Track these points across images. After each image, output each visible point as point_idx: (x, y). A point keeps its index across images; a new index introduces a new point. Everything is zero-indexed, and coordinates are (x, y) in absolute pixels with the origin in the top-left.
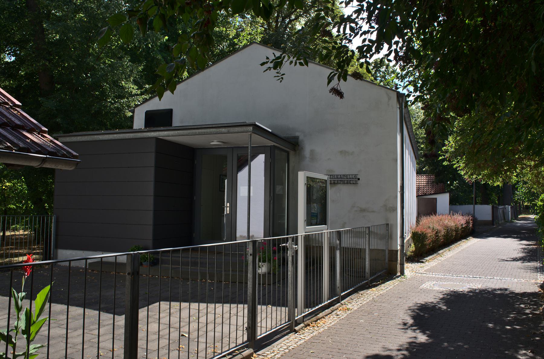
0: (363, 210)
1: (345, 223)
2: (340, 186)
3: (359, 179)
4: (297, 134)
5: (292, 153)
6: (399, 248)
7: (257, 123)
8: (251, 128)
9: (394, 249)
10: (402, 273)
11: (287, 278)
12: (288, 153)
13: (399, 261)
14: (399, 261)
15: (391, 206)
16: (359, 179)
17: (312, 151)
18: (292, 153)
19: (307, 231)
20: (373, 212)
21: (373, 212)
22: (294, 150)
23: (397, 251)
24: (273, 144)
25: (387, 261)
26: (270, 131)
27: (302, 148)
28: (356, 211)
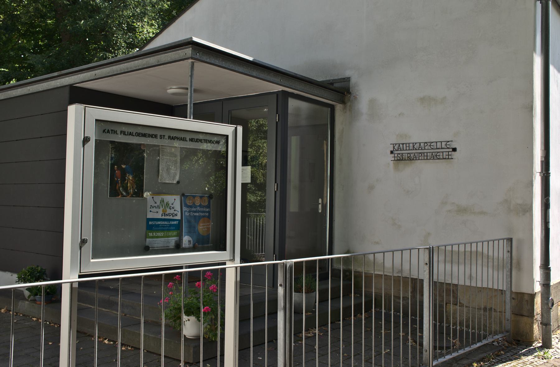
0: (462, 210)
1: (429, 234)
2: (419, 164)
3: (454, 150)
4: (348, 74)
5: (339, 107)
6: (538, 288)
7: (195, 39)
8: (188, 51)
9: (525, 290)
10: (547, 344)
11: (222, 355)
12: (332, 108)
13: (538, 317)
14: (538, 317)
15: (520, 201)
16: (454, 150)
17: (372, 102)
18: (339, 107)
19: (85, 271)
20: (482, 213)
21: (482, 213)
22: (343, 102)
23: (532, 296)
24: (280, 88)
25: (508, 314)
26: (251, 59)
27: (355, 98)
28: (449, 211)
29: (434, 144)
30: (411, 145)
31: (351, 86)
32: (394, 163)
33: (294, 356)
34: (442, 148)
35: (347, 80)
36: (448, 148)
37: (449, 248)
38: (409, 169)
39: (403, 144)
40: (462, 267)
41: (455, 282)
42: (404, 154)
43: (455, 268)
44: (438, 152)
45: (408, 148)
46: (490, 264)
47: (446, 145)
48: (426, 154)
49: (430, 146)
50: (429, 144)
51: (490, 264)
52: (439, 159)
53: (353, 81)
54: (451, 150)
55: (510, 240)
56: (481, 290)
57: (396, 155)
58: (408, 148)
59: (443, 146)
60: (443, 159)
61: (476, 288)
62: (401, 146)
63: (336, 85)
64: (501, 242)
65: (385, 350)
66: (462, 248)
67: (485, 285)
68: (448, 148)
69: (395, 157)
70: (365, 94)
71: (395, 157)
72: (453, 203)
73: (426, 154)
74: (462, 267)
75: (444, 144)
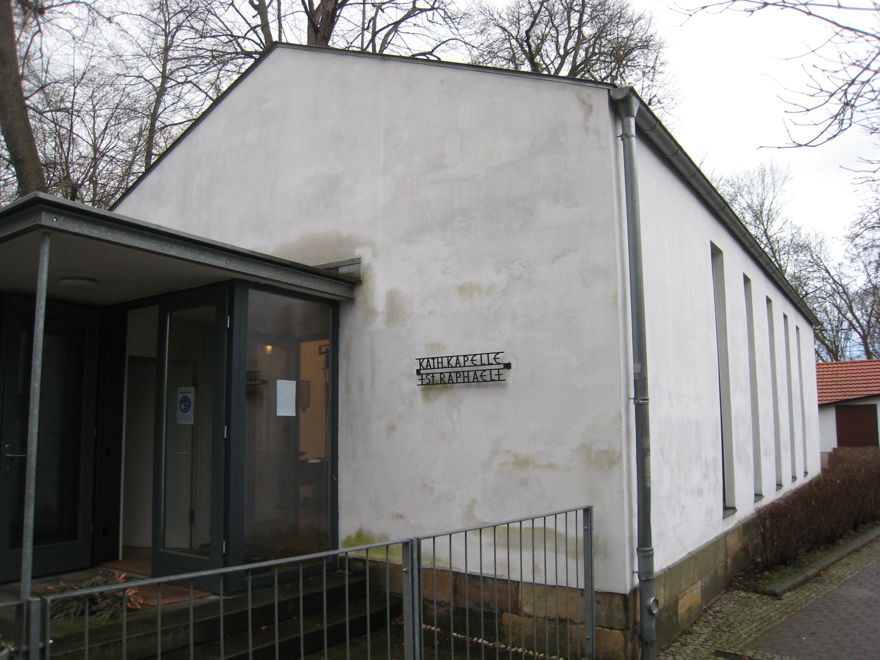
0: (522, 462)
1: (474, 501)
3: (508, 366)
4: (358, 252)
15: (604, 447)
16: (508, 366)
20: (550, 466)
21: (550, 466)
29: (478, 358)
30: (445, 360)
31: (361, 271)
32: (422, 389)
33: (2, 607)
34: (489, 364)
35: (357, 261)
36: (499, 364)
37: (527, 524)
38: (442, 400)
39: (433, 359)
40: (527, 555)
41: (515, 577)
42: (441, 376)
43: (515, 556)
44: (485, 371)
45: (440, 365)
46: (562, 549)
47: (495, 359)
48: (466, 374)
49: (472, 360)
50: (470, 358)
51: (562, 549)
52: (485, 381)
53: (365, 261)
54: (502, 366)
55: (588, 511)
56: (554, 589)
57: (424, 377)
58: (440, 365)
59: (492, 361)
60: (492, 380)
61: (545, 586)
62: (431, 361)
63: (343, 270)
64: (572, 515)
65: (254, 646)
66: (550, 523)
67: (562, 582)
68: (499, 364)
69: (422, 379)
70: (380, 285)
71: (422, 379)
72: (508, 451)
73: (466, 374)
74: (527, 555)
75: (492, 356)
